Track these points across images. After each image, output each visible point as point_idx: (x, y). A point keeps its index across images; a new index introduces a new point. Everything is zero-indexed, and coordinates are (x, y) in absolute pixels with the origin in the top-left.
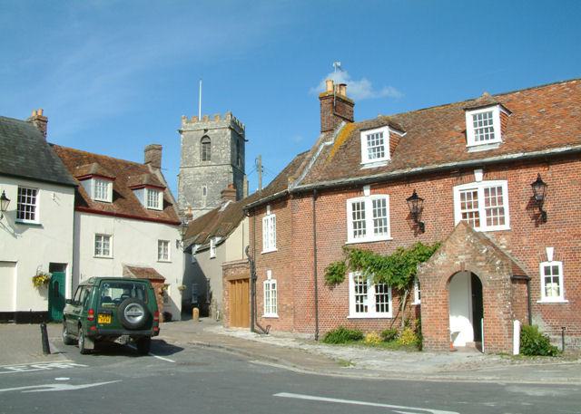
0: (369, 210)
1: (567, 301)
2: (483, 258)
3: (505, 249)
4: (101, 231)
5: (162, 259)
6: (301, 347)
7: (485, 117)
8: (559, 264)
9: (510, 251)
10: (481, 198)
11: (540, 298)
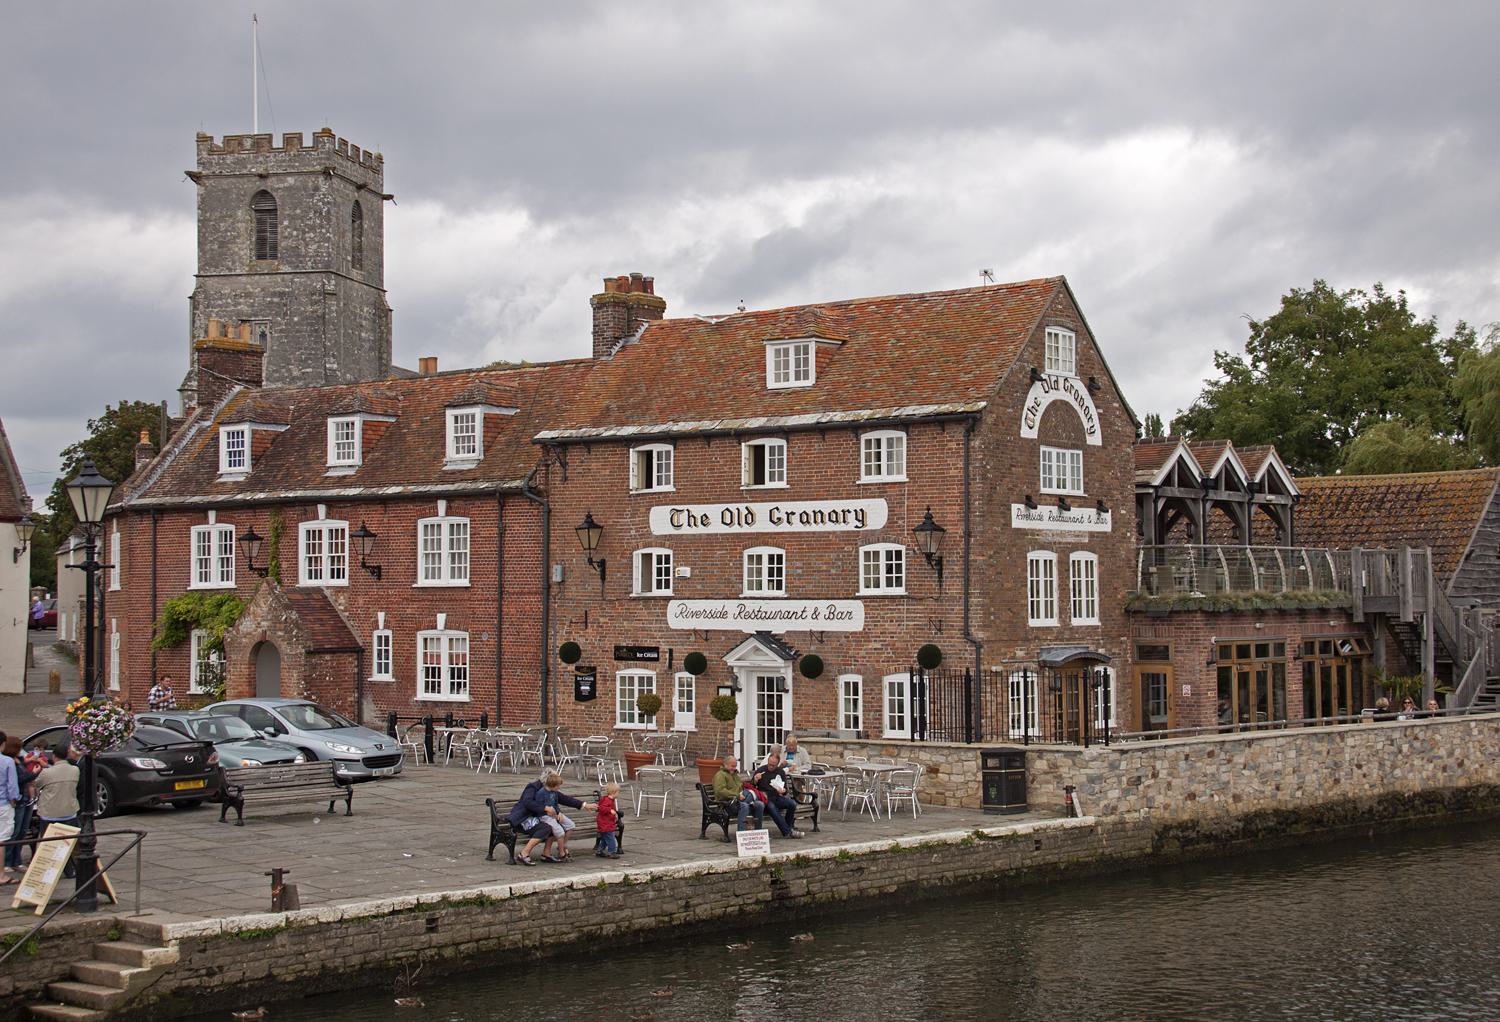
2: (283, 626)
3: (343, 611)
8: (389, 633)
9: (347, 614)
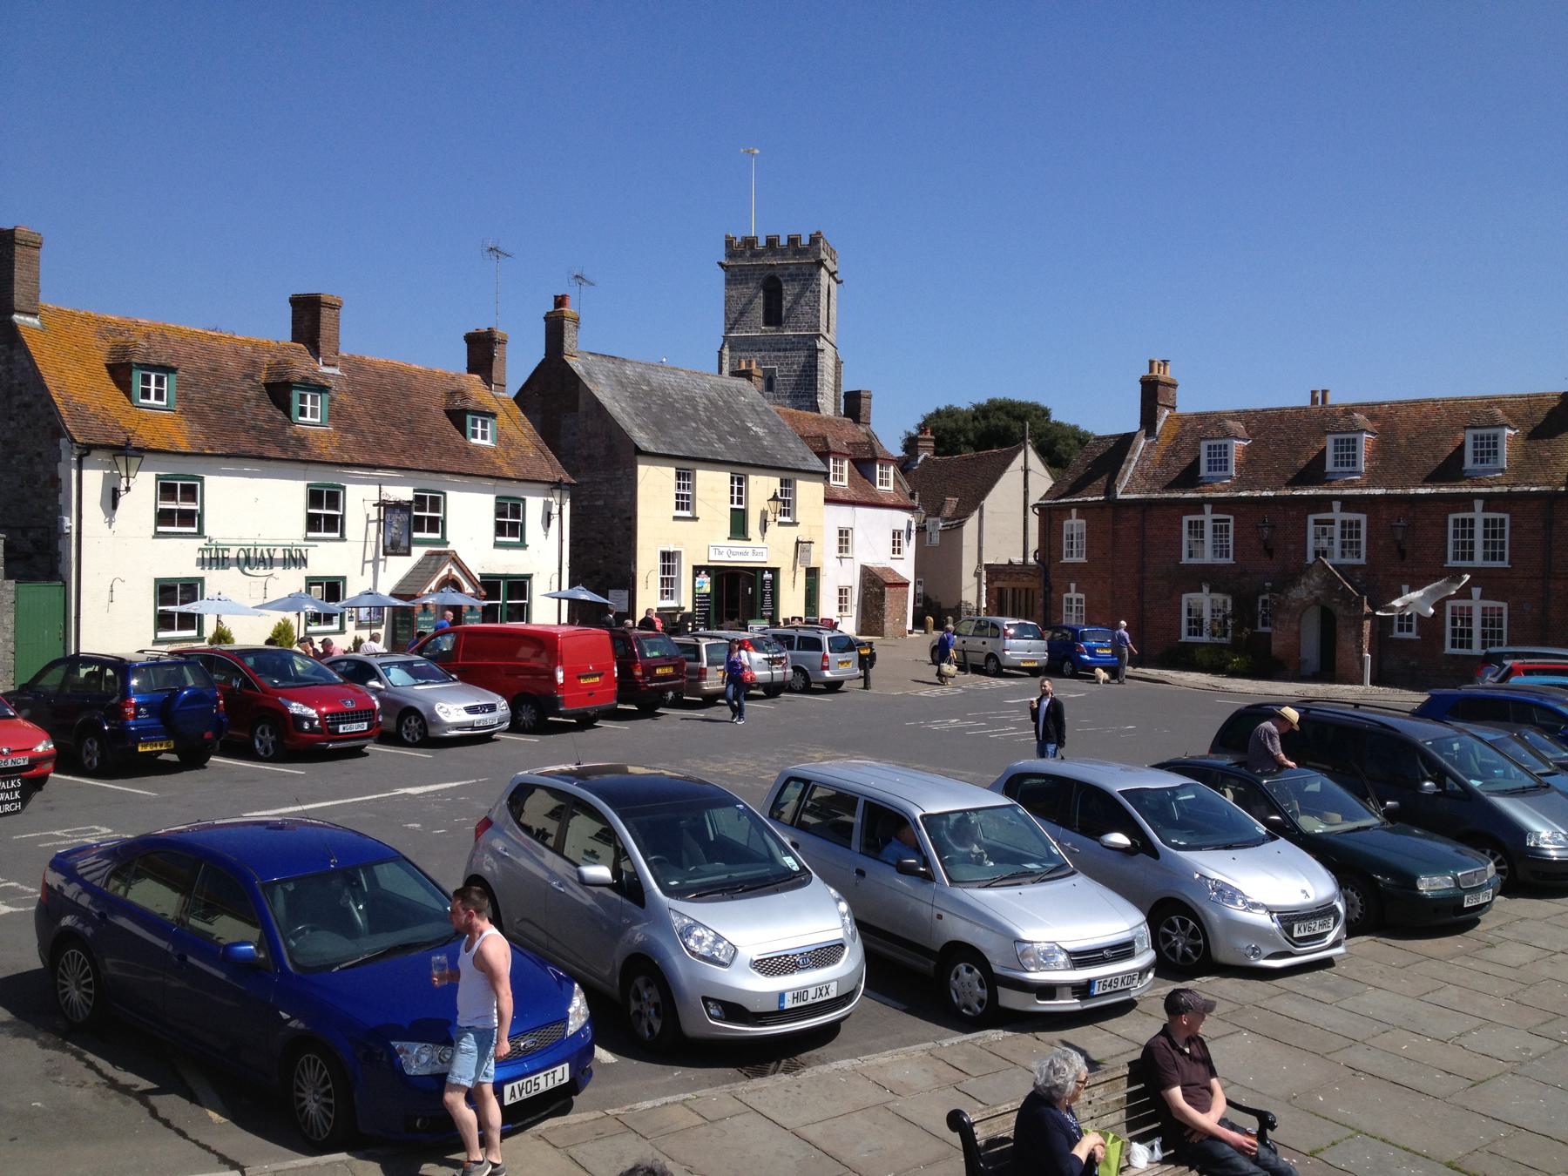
0: (1479, 529)
1: (1419, 637)
3: (1359, 583)
4: (845, 525)
5: (272, 548)
6: (1426, 733)
7: (1220, 448)
9: (1364, 585)
10: (1337, 529)
11: (1392, 633)
